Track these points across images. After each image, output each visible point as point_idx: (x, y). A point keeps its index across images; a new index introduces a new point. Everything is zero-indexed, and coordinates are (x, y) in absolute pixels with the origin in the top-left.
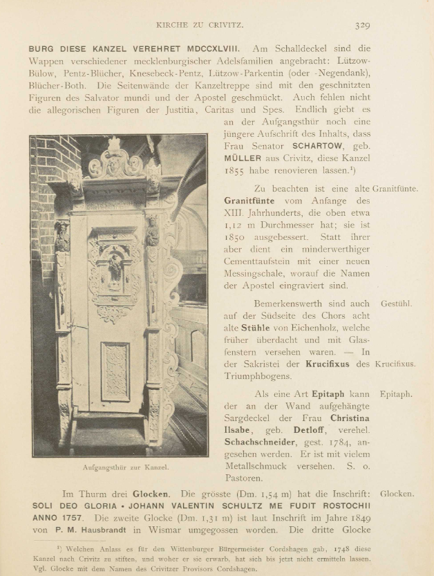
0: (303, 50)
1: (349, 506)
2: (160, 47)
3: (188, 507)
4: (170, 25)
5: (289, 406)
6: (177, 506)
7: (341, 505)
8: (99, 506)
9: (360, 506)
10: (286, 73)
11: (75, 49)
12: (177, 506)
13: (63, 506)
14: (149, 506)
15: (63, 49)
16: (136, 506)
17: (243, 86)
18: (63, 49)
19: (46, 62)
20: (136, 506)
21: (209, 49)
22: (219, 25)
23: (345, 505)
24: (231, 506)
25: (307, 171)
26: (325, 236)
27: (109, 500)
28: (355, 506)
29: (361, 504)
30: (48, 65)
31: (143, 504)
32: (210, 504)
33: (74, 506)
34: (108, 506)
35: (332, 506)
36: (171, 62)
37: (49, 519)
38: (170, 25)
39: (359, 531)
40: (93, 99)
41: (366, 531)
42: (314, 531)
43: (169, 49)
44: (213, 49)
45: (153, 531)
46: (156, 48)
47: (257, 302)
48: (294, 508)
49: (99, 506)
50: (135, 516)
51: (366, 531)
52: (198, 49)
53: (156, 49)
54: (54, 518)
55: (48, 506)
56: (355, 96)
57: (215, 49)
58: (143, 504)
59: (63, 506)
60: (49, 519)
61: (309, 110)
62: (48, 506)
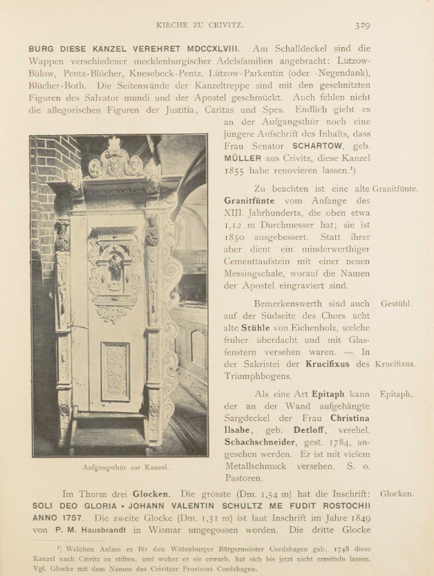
0: (303, 50)
1: (349, 506)
2: (160, 47)
3: (188, 507)
4: (170, 25)
5: (289, 406)
6: (177, 506)
7: (341, 505)
8: (99, 506)
9: (360, 506)
10: (286, 73)
11: (75, 49)
12: (177, 506)
13: (63, 506)
14: (149, 506)
15: (63, 49)
16: (136, 506)
17: (243, 86)
18: (63, 49)
19: (46, 62)
20: (136, 506)
21: (209, 49)
22: (219, 25)
23: (345, 505)
24: (231, 506)
25: (307, 171)
26: (325, 236)
27: (109, 500)
28: (355, 506)
29: (361, 504)
30: (48, 65)
31: (143, 504)
32: (210, 504)
33: (74, 506)
34: (108, 506)
35: (332, 506)
36: (171, 62)
37: (49, 519)
38: (170, 25)
39: (359, 531)
40: (93, 99)
41: (366, 531)
42: (314, 531)
43: (169, 49)
44: (213, 49)
45: (153, 531)
46: (156, 48)
47: (257, 302)
48: (294, 508)
49: (99, 506)
50: (135, 516)
51: (366, 531)
52: (198, 49)
53: (156, 49)
54: (54, 518)
55: (48, 506)
56: (355, 96)
57: (215, 49)
58: (143, 504)
59: (63, 506)
60: (49, 519)
61: (309, 110)
62: (48, 506)
